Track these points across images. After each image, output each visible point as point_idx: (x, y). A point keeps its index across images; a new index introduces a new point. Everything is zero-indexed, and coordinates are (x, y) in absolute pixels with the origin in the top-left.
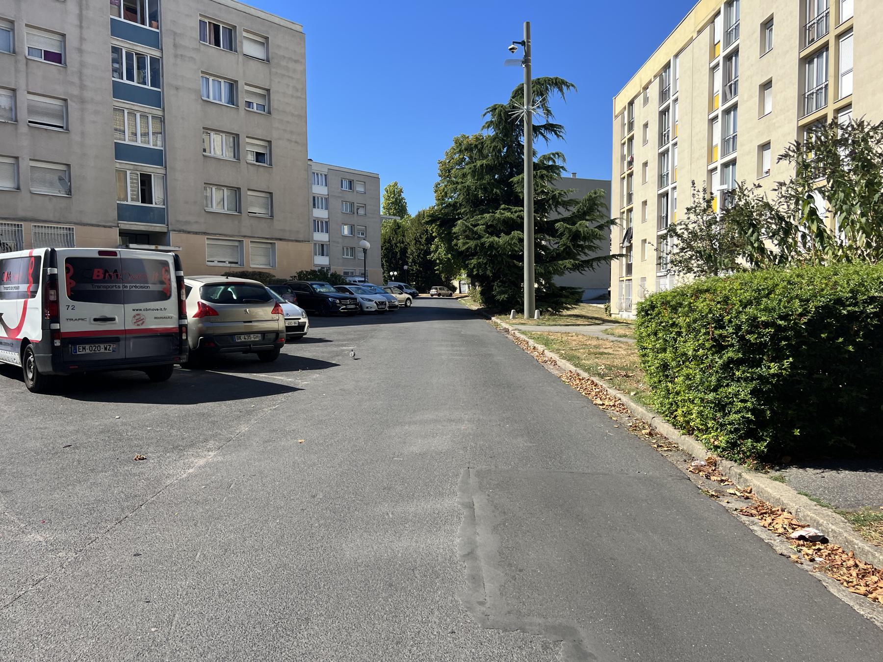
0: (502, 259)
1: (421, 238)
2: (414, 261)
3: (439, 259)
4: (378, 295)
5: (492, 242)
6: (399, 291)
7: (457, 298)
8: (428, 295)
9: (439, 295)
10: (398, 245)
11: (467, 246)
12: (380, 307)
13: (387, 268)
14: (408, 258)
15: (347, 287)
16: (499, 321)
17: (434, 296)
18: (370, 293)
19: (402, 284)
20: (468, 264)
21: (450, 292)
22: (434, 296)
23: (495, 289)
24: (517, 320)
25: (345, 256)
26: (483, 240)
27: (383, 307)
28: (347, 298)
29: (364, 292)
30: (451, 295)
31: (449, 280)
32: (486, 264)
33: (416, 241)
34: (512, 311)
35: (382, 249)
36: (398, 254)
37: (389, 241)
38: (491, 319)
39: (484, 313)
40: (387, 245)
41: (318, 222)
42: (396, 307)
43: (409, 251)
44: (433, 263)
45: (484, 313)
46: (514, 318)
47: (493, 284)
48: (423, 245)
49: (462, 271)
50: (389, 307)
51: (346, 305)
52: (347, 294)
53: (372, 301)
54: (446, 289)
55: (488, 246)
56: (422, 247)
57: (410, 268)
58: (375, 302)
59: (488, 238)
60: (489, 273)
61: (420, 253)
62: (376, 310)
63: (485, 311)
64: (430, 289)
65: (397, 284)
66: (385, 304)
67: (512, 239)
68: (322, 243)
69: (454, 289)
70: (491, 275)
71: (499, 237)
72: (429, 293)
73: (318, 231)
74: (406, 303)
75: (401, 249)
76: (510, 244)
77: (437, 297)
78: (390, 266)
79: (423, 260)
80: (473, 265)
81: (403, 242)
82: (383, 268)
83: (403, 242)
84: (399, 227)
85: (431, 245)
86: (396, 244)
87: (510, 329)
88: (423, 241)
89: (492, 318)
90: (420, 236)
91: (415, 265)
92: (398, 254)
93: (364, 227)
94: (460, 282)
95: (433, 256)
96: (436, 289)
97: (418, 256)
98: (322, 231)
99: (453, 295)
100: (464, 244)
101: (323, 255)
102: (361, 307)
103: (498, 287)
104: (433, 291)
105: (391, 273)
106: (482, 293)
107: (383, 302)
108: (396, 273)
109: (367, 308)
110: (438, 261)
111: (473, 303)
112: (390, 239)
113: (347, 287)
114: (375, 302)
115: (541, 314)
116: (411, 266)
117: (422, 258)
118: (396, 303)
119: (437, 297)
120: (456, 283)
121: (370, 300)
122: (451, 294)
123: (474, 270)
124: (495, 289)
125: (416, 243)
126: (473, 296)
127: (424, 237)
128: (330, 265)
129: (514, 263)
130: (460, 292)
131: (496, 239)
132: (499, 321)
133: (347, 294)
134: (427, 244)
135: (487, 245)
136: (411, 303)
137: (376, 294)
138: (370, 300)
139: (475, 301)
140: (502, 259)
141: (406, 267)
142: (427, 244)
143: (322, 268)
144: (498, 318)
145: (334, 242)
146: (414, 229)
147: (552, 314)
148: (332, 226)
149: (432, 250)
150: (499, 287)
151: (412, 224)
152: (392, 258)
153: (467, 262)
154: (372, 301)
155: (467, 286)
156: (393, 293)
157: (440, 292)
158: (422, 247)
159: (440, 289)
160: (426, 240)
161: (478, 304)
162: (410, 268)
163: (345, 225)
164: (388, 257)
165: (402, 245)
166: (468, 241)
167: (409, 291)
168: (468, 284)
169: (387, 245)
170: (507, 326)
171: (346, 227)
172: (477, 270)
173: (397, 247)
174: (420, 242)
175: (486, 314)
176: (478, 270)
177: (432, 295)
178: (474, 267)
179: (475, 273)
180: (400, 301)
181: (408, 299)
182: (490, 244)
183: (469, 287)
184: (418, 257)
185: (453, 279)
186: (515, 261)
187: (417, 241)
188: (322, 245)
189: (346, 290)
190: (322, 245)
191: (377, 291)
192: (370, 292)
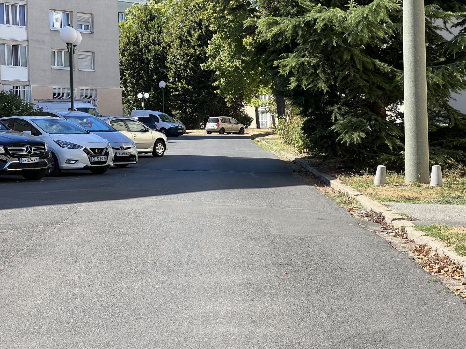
0: (352, 59)
1: (191, 35)
2: (178, 75)
3: (219, 68)
4: (92, 136)
5: (331, 21)
6: (142, 126)
7: (253, 137)
8: (202, 132)
9: (222, 131)
10: (151, 47)
11: (276, 29)
12: (96, 159)
13: (133, 87)
14: (168, 69)
15: (28, 118)
16: (350, 191)
17: (213, 134)
18: (79, 132)
19: (156, 113)
20: (277, 67)
21: (240, 126)
22: (213, 134)
23: (336, 120)
24: (391, 188)
25: (56, 67)
26: (309, 16)
27: (102, 159)
28: (21, 143)
29: (67, 130)
30: (242, 131)
31: (237, 105)
32: (315, 67)
33: (182, 41)
34: (379, 167)
35: (123, 55)
36: (152, 63)
37: (136, 42)
38: (328, 184)
39: (310, 169)
40: (133, 48)
41: (7, 6)
42: (132, 157)
43: (169, 57)
44: (209, 74)
45: (310, 169)
46: (383, 183)
47: (329, 108)
48: (193, 47)
49: (262, 90)
50: (116, 158)
51: (19, 157)
52: (27, 135)
53: (78, 147)
54: (233, 120)
55: (322, 30)
56: (191, 51)
57: (171, 85)
58: (85, 150)
59: (320, 11)
60: (322, 86)
61: (189, 61)
62: (86, 168)
63: (314, 165)
64: (206, 121)
65: (146, 113)
66: (107, 154)
67: (375, 12)
68: (15, 44)
69: (246, 121)
70: (326, 90)
71: (346, 9)
72: (204, 128)
73: (8, 22)
74: (155, 149)
75: (156, 54)
76: (369, 25)
77: (217, 134)
78: (137, 83)
79: (195, 73)
80: (288, 69)
81: (159, 44)
82: (126, 87)
83: (159, 44)
84: (152, 18)
85: (207, 44)
86: (147, 46)
87: (388, 217)
88: (194, 40)
89: (332, 182)
90: (189, 32)
91: (179, 81)
92: (152, 63)
93: (89, 16)
94: (257, 108)
95: (211, 64)
96: (217, 121)
97: (186, 66)
98: (15, 23)
99: (246, 131)
100: (270, 25)
101: (16, 64)
102: (55, 158)
103: (341, 115)
104: (211, 125)
105: (140, 96)
106: (307, 128)
107: (102, 150)
108: (147, 95)
109: (69, 161)
110: (218, 73)
111: (283, 146)
112: (137, 38)
113: (28, 118)
114: (85, 150)
115: (444, 175)
116: (172, 83)
117: (191, 69)
118: (133, 151)
119: (217, 134)
120: (249, 110)
121: (74, 146)
122: (242, 129)
123: (292, 79)
124: (336, 120)
125: (182, 44)
126: (284, 134)
127: (196, 34)
128: (29, 81)
129: (375, 65)
130: (258, 127)
131: (339, 12)
132: (350, 191)
133: (27, 135)
134: (200, 46)
135: (319, 26)
136: (165, 149)
137: (88, 132)
138: (74, 146)
139: (287, 143)
140: (352, 59)
141: (162, 84)
142: (200, 46)
143: (15, 87)
144: (346, 183)
145: (37, 41)
146: (177, 20)
147: (250, 125)
148: (31, 13)
149: (208, 54)
150: (344, 115)
151: (175, 12)
152: (140, 70)
153: (275, 63)
154: (78, 147)
155: (269, 115)
156: (129, 130)
157: (222, 125)
158: (191, 51)
159: (223, 121)
160: (199, 38)
161: (296, 150)
162: (171, 85)
163: (56, 11)
164: (134, 68)
165: (157, 47)
166: (278, 19)
167: (167, 126)
168: (272, 112)
169: (133, 48)
170: (377, 207)
171: (57, 16)
172: (297, 80)
173: (149, 51)
174: (188, 41)
175: (315, 171)
176: (299, 80)
177: (209, 132)
178: (291, 74)
179: (293, 85)
180: (139, 146)
181: (160, 140)
182: (325, 25)
183: (273, 117)
184: (185, 67)
185: (246, 104)
186: (376, 61)
187: (183, 40)
188: (15, 47)
189: (27, 126)
190: (15, 47)
191: (94, 127)
192: (77, 129)
